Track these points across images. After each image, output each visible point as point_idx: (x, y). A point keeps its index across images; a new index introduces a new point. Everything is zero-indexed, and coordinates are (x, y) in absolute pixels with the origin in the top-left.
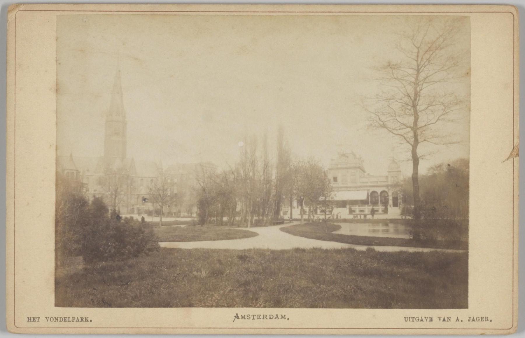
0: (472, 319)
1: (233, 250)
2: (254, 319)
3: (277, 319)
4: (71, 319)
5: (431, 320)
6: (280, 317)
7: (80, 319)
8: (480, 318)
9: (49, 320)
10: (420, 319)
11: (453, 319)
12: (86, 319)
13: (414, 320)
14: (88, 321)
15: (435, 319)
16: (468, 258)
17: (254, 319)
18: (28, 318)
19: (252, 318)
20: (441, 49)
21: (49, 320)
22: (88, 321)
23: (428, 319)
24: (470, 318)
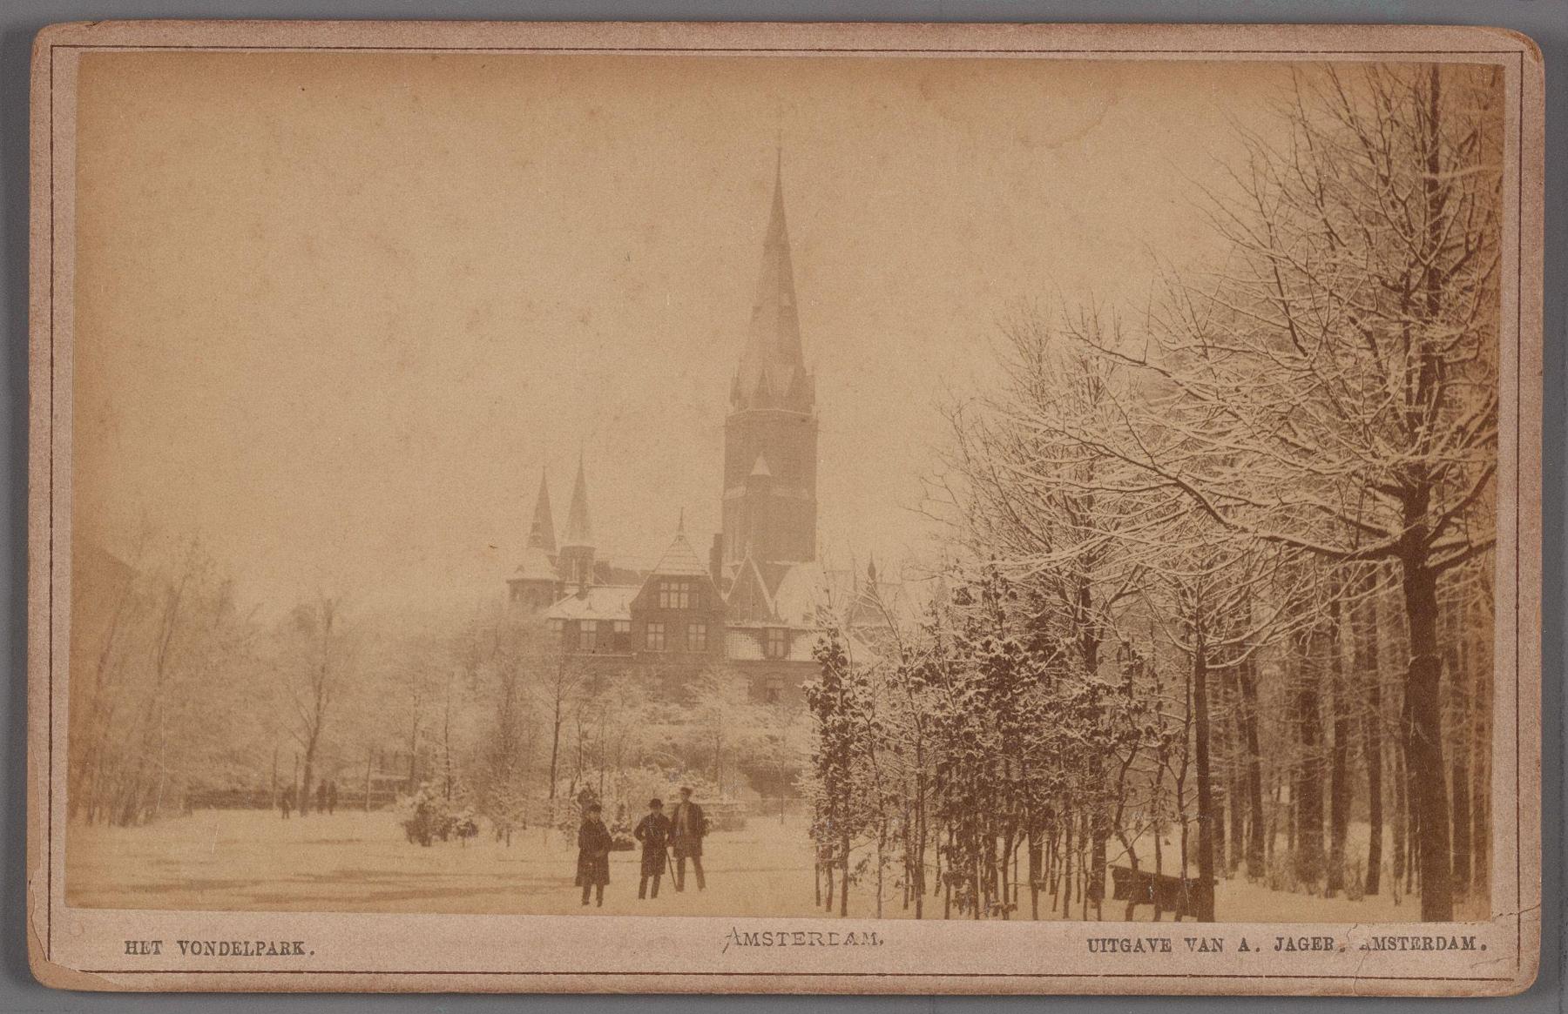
0: (1285, 943)
1: (1212, 895)
2: (783, 944)
3: (850, 946)
4: (252, 947)
5: (1166, 949)
6: (1460, 943)
7: (1460, 943)
8: (1311, 942)
9: (188, 950)
10: (1134, 944)
11: (1231, 945)
12: (297, 945)
13: (1118, 947)
14: (301, 952)
15: (1178, 946)
16: (28, 192)
17: (783, 944)
18: (128, 943)
19: (777, 940)
20: (1253, 720)
21: (188, 950)
22: (301, 952)
23: (1159, 946)
24: (1280, 939)
